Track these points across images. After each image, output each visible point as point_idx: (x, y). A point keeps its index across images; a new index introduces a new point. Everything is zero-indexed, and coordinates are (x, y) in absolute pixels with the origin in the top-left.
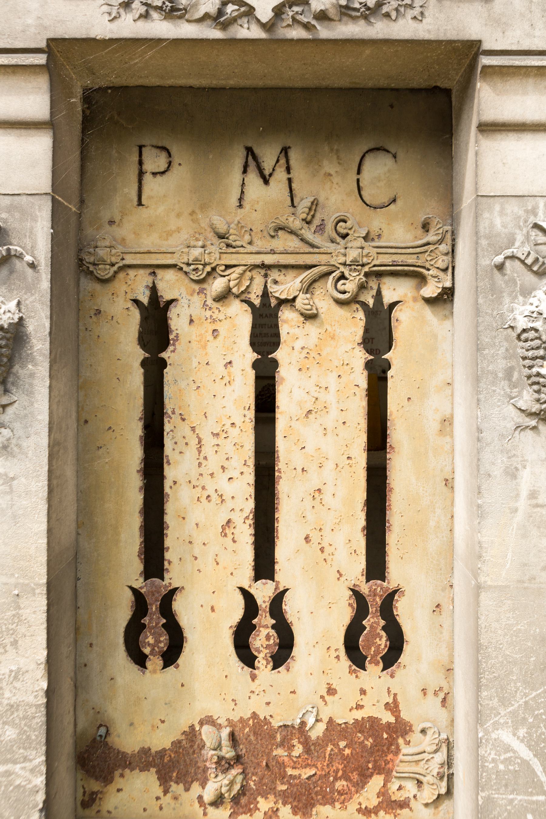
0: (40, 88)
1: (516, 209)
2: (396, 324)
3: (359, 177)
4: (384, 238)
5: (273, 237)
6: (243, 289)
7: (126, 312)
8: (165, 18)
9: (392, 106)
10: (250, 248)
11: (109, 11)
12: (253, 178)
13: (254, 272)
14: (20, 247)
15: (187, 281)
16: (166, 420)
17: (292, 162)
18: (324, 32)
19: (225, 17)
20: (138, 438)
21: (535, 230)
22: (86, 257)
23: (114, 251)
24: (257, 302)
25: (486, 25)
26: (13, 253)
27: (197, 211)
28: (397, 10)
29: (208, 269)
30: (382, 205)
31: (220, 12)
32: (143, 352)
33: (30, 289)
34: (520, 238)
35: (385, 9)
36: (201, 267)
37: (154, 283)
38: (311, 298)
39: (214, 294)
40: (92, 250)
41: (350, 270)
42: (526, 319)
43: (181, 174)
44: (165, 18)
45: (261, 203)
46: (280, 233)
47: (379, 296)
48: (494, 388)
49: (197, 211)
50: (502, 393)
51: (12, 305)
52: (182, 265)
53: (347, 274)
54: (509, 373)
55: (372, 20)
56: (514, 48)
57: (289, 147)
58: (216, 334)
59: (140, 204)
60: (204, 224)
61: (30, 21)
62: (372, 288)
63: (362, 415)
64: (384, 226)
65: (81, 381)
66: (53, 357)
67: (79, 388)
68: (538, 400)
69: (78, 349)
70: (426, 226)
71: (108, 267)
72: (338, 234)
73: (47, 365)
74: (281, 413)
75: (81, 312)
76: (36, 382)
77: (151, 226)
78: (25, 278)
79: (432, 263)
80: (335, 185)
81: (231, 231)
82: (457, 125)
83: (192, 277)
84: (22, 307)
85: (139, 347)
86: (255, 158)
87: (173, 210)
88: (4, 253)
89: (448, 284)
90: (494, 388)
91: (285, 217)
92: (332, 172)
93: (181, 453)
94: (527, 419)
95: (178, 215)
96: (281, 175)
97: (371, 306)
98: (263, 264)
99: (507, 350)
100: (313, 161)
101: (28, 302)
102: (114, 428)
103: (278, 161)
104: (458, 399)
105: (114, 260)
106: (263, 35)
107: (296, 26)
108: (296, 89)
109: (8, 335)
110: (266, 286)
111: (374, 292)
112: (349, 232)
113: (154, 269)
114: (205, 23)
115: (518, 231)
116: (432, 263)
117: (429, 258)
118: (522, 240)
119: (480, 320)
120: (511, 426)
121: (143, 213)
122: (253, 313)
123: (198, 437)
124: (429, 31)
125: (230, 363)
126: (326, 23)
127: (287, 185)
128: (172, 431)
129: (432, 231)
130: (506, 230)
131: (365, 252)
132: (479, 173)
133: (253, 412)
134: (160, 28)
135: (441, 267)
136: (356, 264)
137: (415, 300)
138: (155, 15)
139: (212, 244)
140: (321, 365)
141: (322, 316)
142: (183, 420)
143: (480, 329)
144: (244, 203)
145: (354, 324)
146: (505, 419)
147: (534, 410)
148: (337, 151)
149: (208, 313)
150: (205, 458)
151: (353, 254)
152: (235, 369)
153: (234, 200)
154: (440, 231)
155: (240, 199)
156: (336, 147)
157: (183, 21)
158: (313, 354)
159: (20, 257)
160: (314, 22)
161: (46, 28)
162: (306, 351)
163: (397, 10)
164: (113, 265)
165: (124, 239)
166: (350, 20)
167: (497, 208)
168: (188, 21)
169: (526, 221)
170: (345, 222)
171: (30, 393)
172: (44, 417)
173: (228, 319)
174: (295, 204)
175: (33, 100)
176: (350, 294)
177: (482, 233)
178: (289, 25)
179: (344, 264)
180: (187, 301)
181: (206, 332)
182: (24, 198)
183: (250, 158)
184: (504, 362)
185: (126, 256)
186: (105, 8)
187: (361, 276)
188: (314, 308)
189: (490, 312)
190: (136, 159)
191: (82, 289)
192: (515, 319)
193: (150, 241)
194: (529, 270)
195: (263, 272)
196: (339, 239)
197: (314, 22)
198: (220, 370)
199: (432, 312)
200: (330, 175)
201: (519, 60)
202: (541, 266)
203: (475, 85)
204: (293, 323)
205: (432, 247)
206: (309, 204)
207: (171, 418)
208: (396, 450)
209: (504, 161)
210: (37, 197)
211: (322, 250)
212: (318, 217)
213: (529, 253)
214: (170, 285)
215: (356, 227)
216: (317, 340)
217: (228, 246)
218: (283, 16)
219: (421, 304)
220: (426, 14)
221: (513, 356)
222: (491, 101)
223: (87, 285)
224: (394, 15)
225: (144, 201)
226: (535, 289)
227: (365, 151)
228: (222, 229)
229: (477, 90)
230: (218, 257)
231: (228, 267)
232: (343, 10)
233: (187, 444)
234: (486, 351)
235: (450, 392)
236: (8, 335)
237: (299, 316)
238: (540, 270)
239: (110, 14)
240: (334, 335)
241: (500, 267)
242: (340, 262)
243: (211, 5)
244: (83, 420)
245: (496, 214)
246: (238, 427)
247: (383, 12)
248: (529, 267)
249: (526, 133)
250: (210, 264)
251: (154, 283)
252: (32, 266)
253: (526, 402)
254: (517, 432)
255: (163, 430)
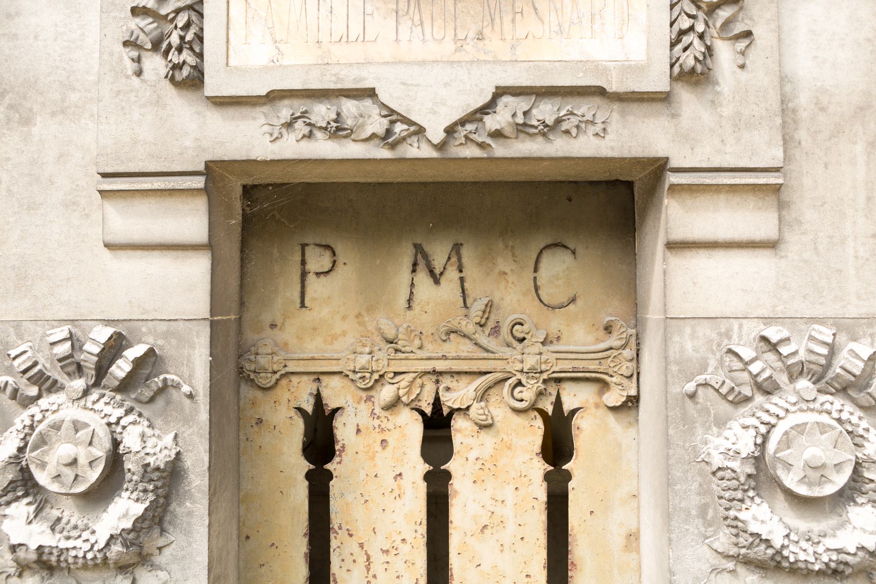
0: (198, 210)
1: (708, 332)
2: (577, 432)
3: (536, 275)
4: (562, 341)
5: (444, 341)
6: (413, 397)
7: (288, 421)
8: (330, 138)
9: (570, 200)
10: (420, 354)
11: (271, 131)
12: (423, 279)
13: (425, 378)
14: (177, 375)
15: (353, 388)
16: (332, 536)
17: (465, 260)
18: (500, 150)
19: (394, 138)
20: (302, 555)
21: (729, 355)
22: (247, 365)
23: (276, 358)
24: (428, 410)
25: (673, 141)
26: (169, 383)
27: (364, 313)
28: (578, 127)
29: (376, 376)
30: (560, 305)
31: (389, 132)
32: (308, 464)
33: (187, 421)
34: (713, 363)
35: (565, 126)
36: (368, 375)
37: (318, 390)
38: (486, 406)
39: (383, 403)
40: (252, 357)
41: (528, 378)
42: (721, 456)
43: (346, 274)
44: (330, 138)
45: (431, 305)
46: (452, 336)
47: (558, 404)
48: (687, 527)
49: (364, 313)
50: (696, 532)
51: (168, 439)
52: (348, 373)
53: (524, 381)
54: (703, 510)
55: (551, 137)
56: (704, 165)
57: (462, 244)
58: (384, 444)
59: (303, 305)
60: (371, 327)
61: (187, 143)
62: (550, 394)
63: (541, 529)
64: (562, 328)
65: (242, 494)
66: (212, 491)
67: (239, 502)
68: (736, 545)
69: (239, 460)
70: (608, 329)
71: (269, 375)
72: (514, 337)
73: (206, 502)
74: (455, 528)
75: (241, 421)
76: (194, 520)
77: (315, 329)
78: (182, 409)
79: (616, 369)
80: (510, 285)
81: (400, 336)
82: (641, 225)
83: (358, 385)
84: (179, 440)
85: (303, 458)
86: (425, 256)
87: (338, 313)
88: (160, 385)
89: (633, 392)
90: (687, 527)
91: (457, 321)
92: (507, 271)
93: (348, 570)
94: (724, 561)
95: (344, 318)
96: (452, 274)
97: (550, 413)
98: (434, 371)
99: (700, 485)
100: (487, 258)
101: (185, 435)
102: (276, 544)
103: (449, 258)
104: (644, 517)
105: (275, 368)
106: (434, 154)
107: (469, 143)
108: (468, 183)
109: (165, 474)
110: (437, 393)
111: (553, 399)
112: (526, 336)
113: (318, 377)
114: (372, 142)
115: (710, 356)
116: (616, 369)
117: (612, 365)
118: (715, 365)
119: (671, 452)
120: (706, 568)
121: (307, 316)
122: (424, 421)
123: (366, 554)
124: (612, 148)
125: (400, 474)
126: (502, 140)
127: (459, 284)
128: (339, 547)
129: (615, 335)
130: (698, 355)
131: (544, 357)
132: (668, 294)
133: (425, 527)
134: (324, 148)
135: (625, 374)
136: (534, 372)
137: (597, 406)
138: (319, 134)
139: (380, 350)
140: (497, 474)
141: (498, 425)
142: (351, 535)
143: (671, 462)
144: (414, 305)
145: (533, 433)
146: (699, 560)
147: (731, 553)
148: (512, 247)
149: (376, 422)
150: (375, 576)
151: (530, 362)
152: (406, 482)
153: (402, 302)
154: (624, 335)
155: (409, 301)
156: (511, 244)
157: (349, 140)
158: (487, 465)
159: (177, 387)
160: (489, 141)
161: (204, 150)
162: (480, 462)
163: (578, 127)
164: (275, 372)
165: (286, 344)
166: (528, 137)
167: (688, 330)
168: (353, 140)
169: (719, 345)
170: (522, 324)
171: (188, 533)
172: (203, 558)
173: (398, 429)
174: (468, 305)
175: (191, 222)
176: (527, 403)
177: (672, 358)
178: (461, 144)
179: (522, 371)
180: (353, 410)
181: (374, 442)
182: (181, 323)
183: (419, 256)
184: (698, 498)
185: (289, 363)
186: (266, 128)
187: (539, 384)
188: (489, 418)
189: (682, 444)
190: (298, 258)
191: (242, 396)
192: (709, 454)
193: (313, 346)
194: (724, 401)
195: (434, 378)
196: (515, 343)
197: (489, 141)
198: (390, 482)
199: (616, 419)
200: (505, 273)
201: (709, 178)
202: (736, 396)
203: (661, 203)
204: (467, 433)
205: (615, 353)
206: (483, 307)
207: (337, 534)
208: (578, 567)
209: (695, 280)
210: (194, 322)
211: (497, 356)
212: (493, 318)
213: (724, 382)
214: (335, 393)
215: (534, 331)
216: (492, 450)
217: (397, 351)
218: (456, 135)
219: (602, 411)
220: (609, 130)
221: (707, 492)
222: (676, 217)
223: (246, 391)
224: (574, 132)
225: (307, 303)
226: (730, 419)
227: (542, 247)
228: (390, 334)
229: (664, 206)
230: (386, 364)
231: (396, 374)
232: (520, 128)
233: (354, 561)
234: (678, 487)
235: (636, 505)
236: (165, 474)
237: (473, 425)
238: (736, 400)
239: (271, 135)
240: (511, 445)
241: (692, 396)
242: (517, 369)
243: (378, 126)
244: (244, 536)
245: (686, 337)
246: (409, 543)
247: (563, 129)
248: (724, 397)
249: (717, 250)
250: (377, 371)
251: (318, 390)
252: (191, 396)
253: (723, 544)
254: (713, 575)
255: (329, 546)
